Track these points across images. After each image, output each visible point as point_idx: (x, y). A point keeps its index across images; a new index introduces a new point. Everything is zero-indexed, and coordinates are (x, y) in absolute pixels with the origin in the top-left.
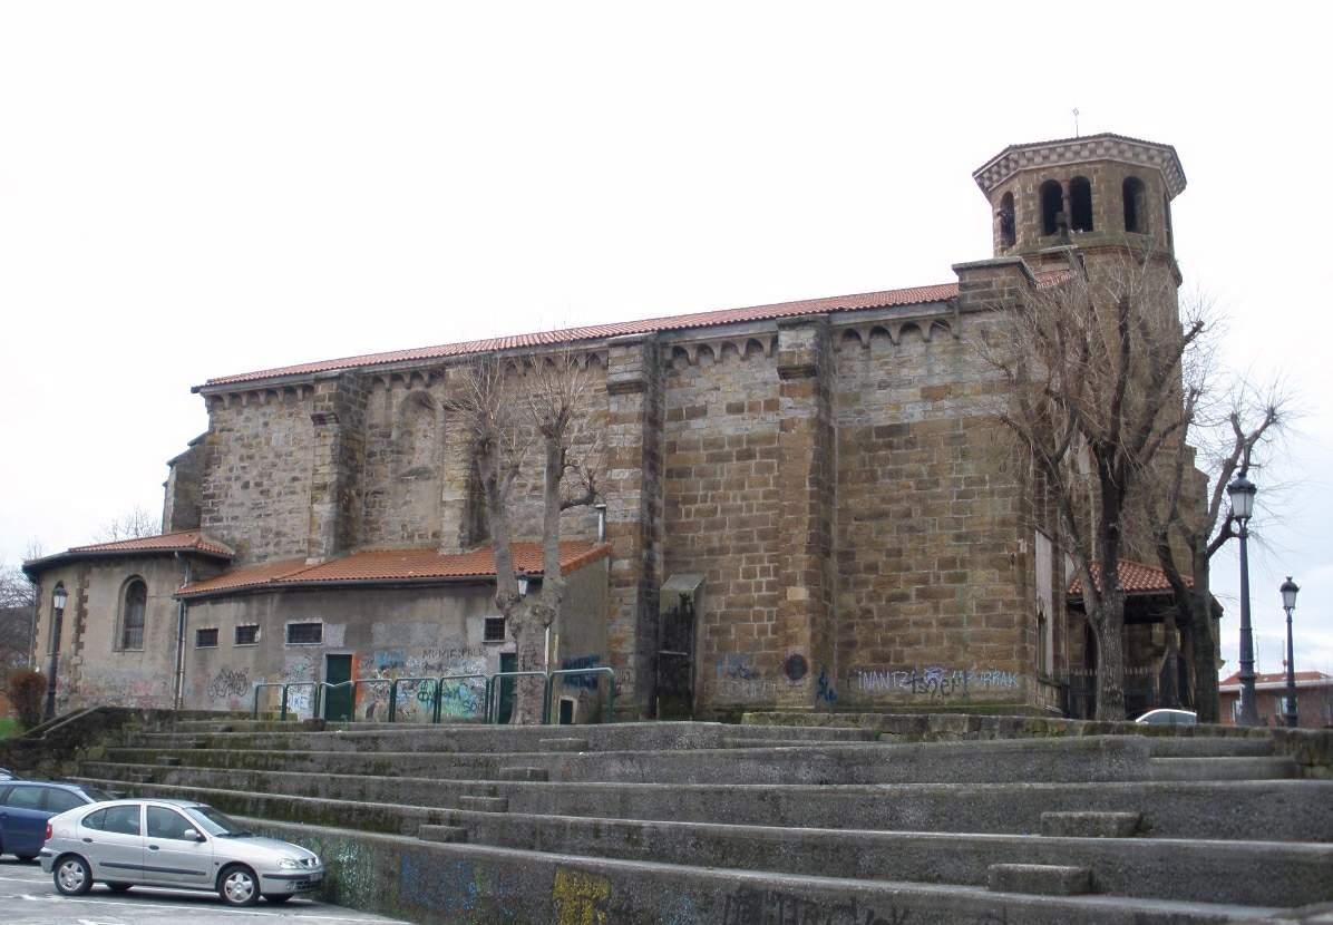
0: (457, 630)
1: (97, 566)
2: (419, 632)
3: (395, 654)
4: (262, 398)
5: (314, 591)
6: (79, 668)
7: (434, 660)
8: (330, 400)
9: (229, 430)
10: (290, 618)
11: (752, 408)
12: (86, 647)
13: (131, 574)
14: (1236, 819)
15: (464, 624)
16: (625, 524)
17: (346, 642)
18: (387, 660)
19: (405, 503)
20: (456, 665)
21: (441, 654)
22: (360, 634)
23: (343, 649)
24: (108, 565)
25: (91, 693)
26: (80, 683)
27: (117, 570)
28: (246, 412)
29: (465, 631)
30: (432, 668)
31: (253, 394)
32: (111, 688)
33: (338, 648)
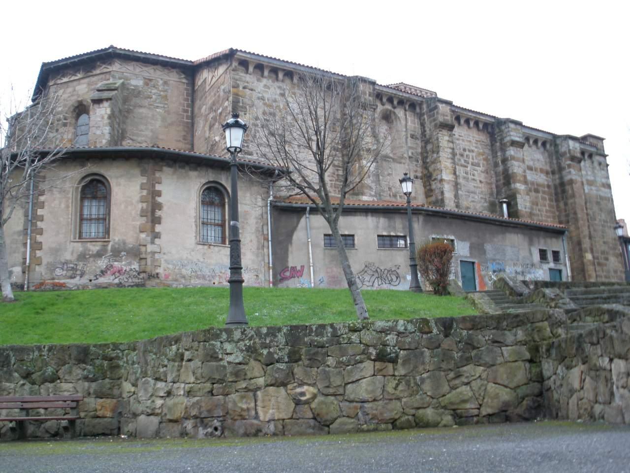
0: (527, 254)
1: (169, 166)
2: (509, 252)
3: (499, 264)
4: (281, 75)
5: (446, 217)
6: (157, 256)
7: (519, 269)
8: (370, 95)
9: (252, 90)
10: (432, 233)
11: (536, 170)
12: (164, 236)
13: (211, 180)
14: (52, 360)
15: (530, 250)
16: (526, 212)
17: (471, 253)
18: (496, 267)
19: (389, 175)
20: (530, 273)
21: (522, 266)
22: (477, 248)
23: (469, 257)
24: (183, 167)
25: (176, 280)
26: (160, 270)
27: (193, 174)
28: (265, 81)
29: (531, 254)
30: (519, 273)
31: (275, 71)
32: (198, 277)
33: (466, 257)
